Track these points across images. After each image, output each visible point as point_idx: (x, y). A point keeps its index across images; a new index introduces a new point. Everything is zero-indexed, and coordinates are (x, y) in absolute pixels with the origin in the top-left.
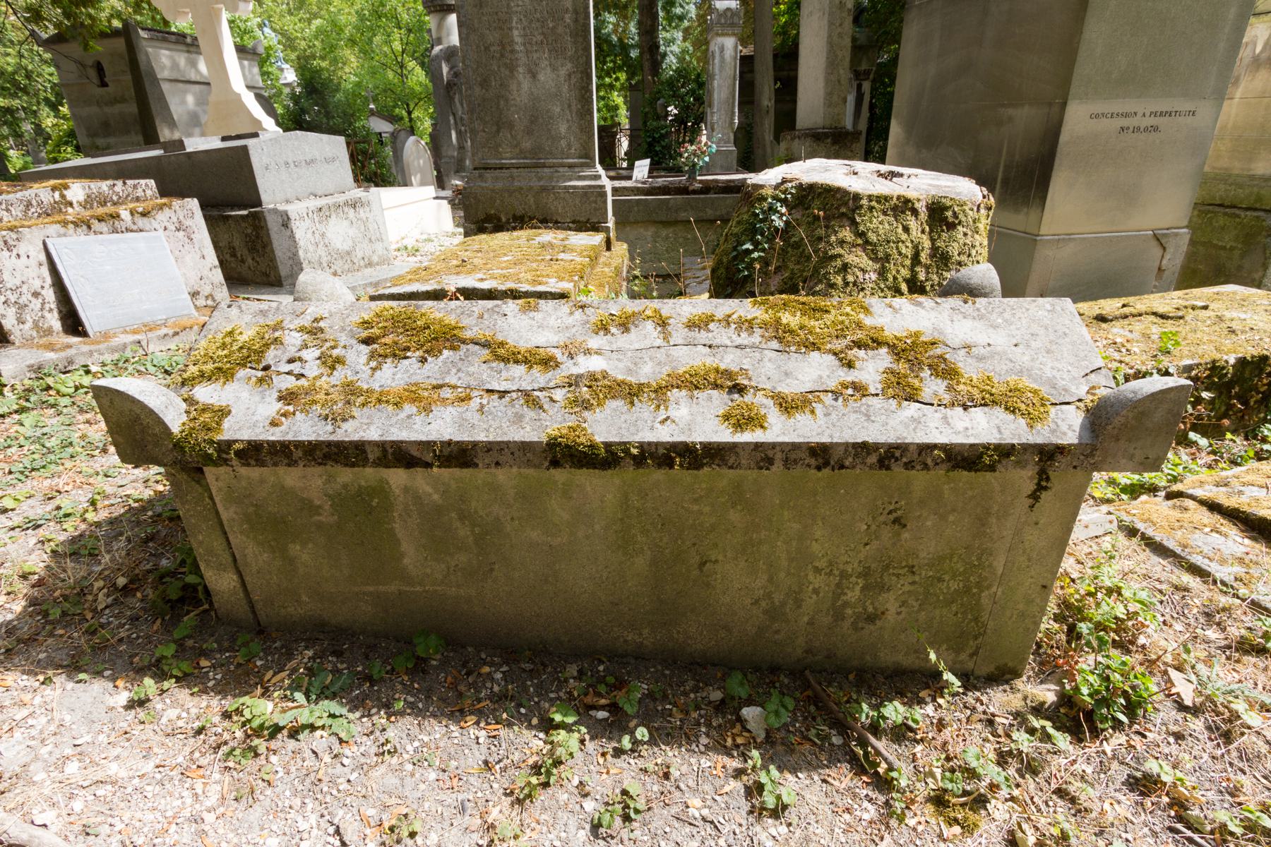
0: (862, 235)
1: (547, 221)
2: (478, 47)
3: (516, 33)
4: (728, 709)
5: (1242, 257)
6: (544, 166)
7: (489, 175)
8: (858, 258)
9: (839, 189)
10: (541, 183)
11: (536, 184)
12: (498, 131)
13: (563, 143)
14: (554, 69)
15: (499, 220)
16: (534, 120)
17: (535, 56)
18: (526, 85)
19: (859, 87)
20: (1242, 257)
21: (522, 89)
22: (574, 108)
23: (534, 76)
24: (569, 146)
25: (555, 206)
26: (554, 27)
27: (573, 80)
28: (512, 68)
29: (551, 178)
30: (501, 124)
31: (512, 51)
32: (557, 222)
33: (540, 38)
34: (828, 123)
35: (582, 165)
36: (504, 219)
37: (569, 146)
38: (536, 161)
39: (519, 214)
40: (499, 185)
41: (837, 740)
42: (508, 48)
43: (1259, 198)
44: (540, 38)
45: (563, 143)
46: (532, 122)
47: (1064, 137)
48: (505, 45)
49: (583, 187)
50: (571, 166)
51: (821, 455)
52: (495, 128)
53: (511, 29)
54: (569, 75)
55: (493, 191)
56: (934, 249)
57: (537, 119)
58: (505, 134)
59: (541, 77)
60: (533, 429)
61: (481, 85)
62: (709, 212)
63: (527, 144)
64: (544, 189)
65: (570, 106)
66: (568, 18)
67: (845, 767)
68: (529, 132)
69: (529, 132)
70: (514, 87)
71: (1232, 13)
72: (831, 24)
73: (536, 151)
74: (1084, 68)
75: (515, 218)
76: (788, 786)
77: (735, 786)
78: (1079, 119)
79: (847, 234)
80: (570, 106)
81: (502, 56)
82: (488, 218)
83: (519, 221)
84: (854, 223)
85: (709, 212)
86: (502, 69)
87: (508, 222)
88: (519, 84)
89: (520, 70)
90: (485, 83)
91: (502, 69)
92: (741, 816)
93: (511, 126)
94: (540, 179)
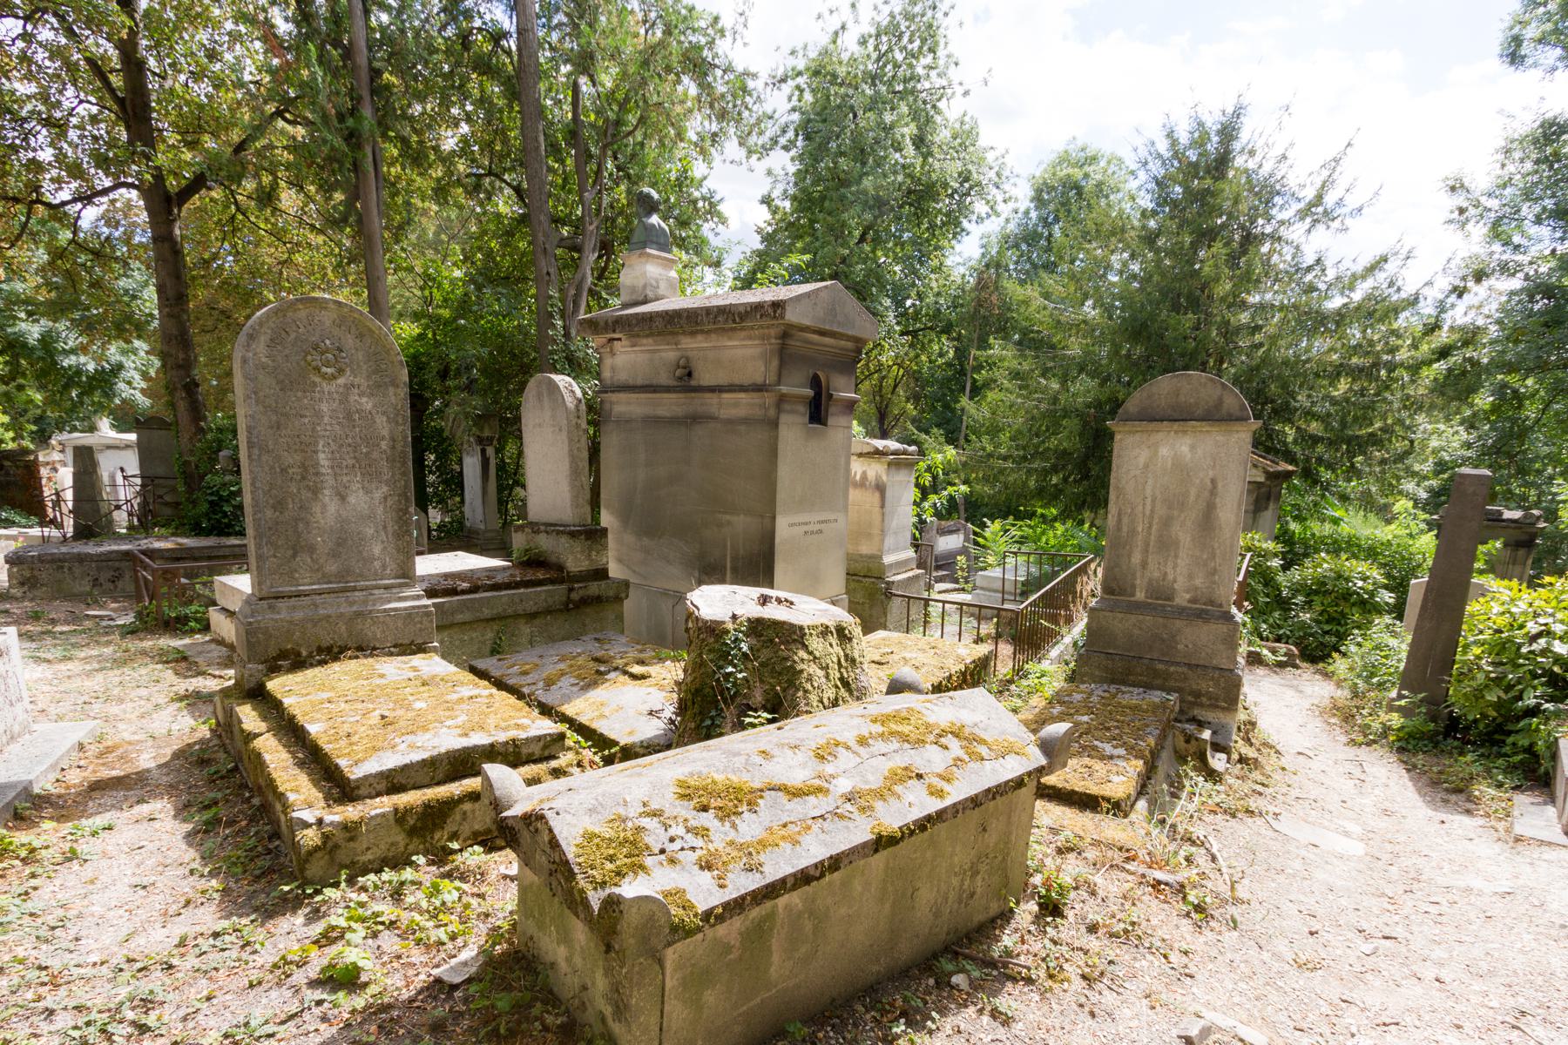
0: (811, 653)
1: (364, 649)
2: (272, 468)
3: (321, 456)
4: (943, 983)
5: (871, 607)
6: (354, 589)
7: (282, 605)
8: (813, 669)
9: (784, 623)
10: (355, 608)
11: (345, 609)
12: (294, 556)
13: (377, 564)
14: (367, 492)
15: (299, 654)
16: (341, 542)
17: (345, 479)
18: (333, 507)
19: (483, 451)
20: (871, 607)
21: (327, 512)
22: (390, 529)
23: (343, 498)
24: (384, 567)
25: (372, 632)
26: (367, 454)
27: (389, 503)
28: (316, 491)
29: (365, 602)
30: (298, 547)
31: (317, 474)
32: (374, 649)
33: (351, 462)
34: (577, 521)
35: (400, 586)
36: (304, 653)
37: (384, 567)
38: (343, 584)
39: (325, 644)
40: (299, 615)
41: (995, 973)
42: (312, 471)
43: (869, 570)
44: (351, 462)
45: (377, 564)
46: (339, 545)
47: (777, 540)
48: (308, 470)
49: (406, 609)
50: (386, 587)
51: (975, 802)
52: (290, 552)
53: (316, 452)
54: (385, 498)
55: (291, 622)
56: (846, 656)
57: (343, 541)
58: (304, 559)
59: (352, 499)
60: (859, 832)
61: (274, 508)
62: (486, 611)
63: (332, 568)
64: (359, 614)
65: (385, 527)
66: (384, 445)
67: (1009, 985)
68: (334, 555)
69: (334, 555)
70: (317, 509)
71: (843, 461)
72: (570, 440)
73: (342, 576)
74: (781, 496)
75: (320, 650)
76: (1003, 1002)
77: (986, 1019)
78: (785, 528)
79: (802, 654)
80: (385, 527)
81: (303, 478)
82: (283, 655)
83: (330, 654)
84: (805, 647)
85: (486, 611)
86: (303, 492)
87: (310, 656)
88: (324, 506)
89: (326, 492)
90: (279, 505)
91: (303, 492)
92: (1002, 1030)
93: (311, 549)
94: (352, 604)
